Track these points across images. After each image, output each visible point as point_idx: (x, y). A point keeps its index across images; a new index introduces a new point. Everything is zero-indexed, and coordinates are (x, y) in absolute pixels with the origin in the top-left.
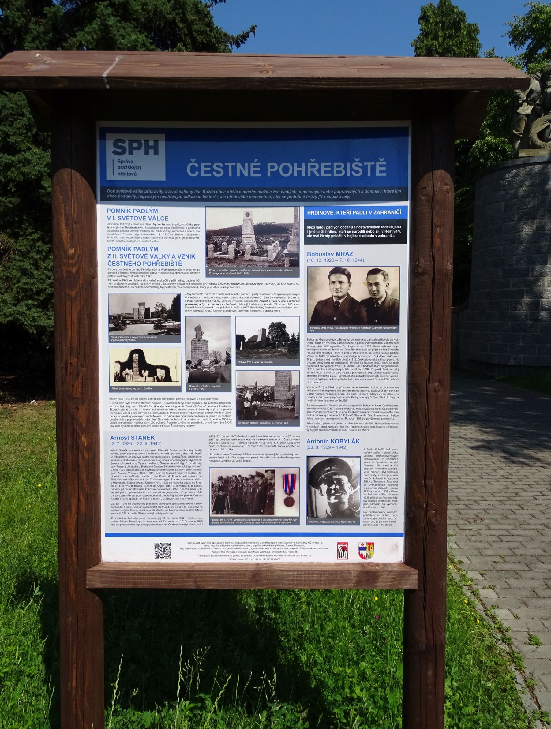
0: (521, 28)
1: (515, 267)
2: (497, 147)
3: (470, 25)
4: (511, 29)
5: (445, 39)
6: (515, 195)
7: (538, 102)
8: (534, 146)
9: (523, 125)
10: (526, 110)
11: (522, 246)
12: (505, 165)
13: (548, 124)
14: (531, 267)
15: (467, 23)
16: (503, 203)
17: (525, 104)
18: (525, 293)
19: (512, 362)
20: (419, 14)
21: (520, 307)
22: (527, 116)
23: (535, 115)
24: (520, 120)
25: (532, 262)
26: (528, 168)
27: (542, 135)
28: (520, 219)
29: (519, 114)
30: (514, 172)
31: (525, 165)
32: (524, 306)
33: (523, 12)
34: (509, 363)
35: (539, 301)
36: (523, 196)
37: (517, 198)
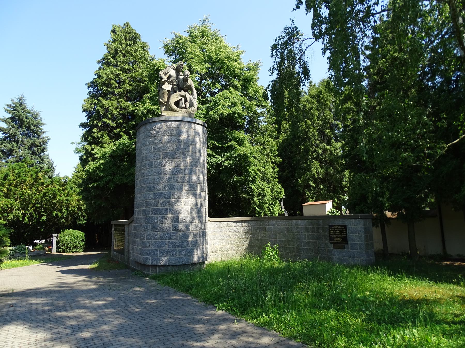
0: (170, 45)
1: (161, 191)
2: (154, 112)
3: (143, 43)
4: (164, 45)
5: (126, 45)
6: (160, 142)
7: (175, 83)
8: (172, 110)
9: (166, 97)
10: (167, 87)
11: (166, 177)
12: (154, 120)
13: (181, 98)
14: (172, 191)
15: (142, 41)
16: (153, 146)
17: (167, 83)
18: (169, 211)
19: (162, 263)
20: (111, 28)
21: (166, 221)
22: (169, 91)
23: (173, 91)
24: (163, 93)
25: (172, 188)
26: (169, 124)
27: (177, 104)
28: (164, 158)
29: (163, 89)
30: (159, 125)
31: (166, 121)
32: (168, 220)
33: (172, 37)
34: (159, 264)
35: (178, 217)
36: (165, 142)
37: (162, 143)
